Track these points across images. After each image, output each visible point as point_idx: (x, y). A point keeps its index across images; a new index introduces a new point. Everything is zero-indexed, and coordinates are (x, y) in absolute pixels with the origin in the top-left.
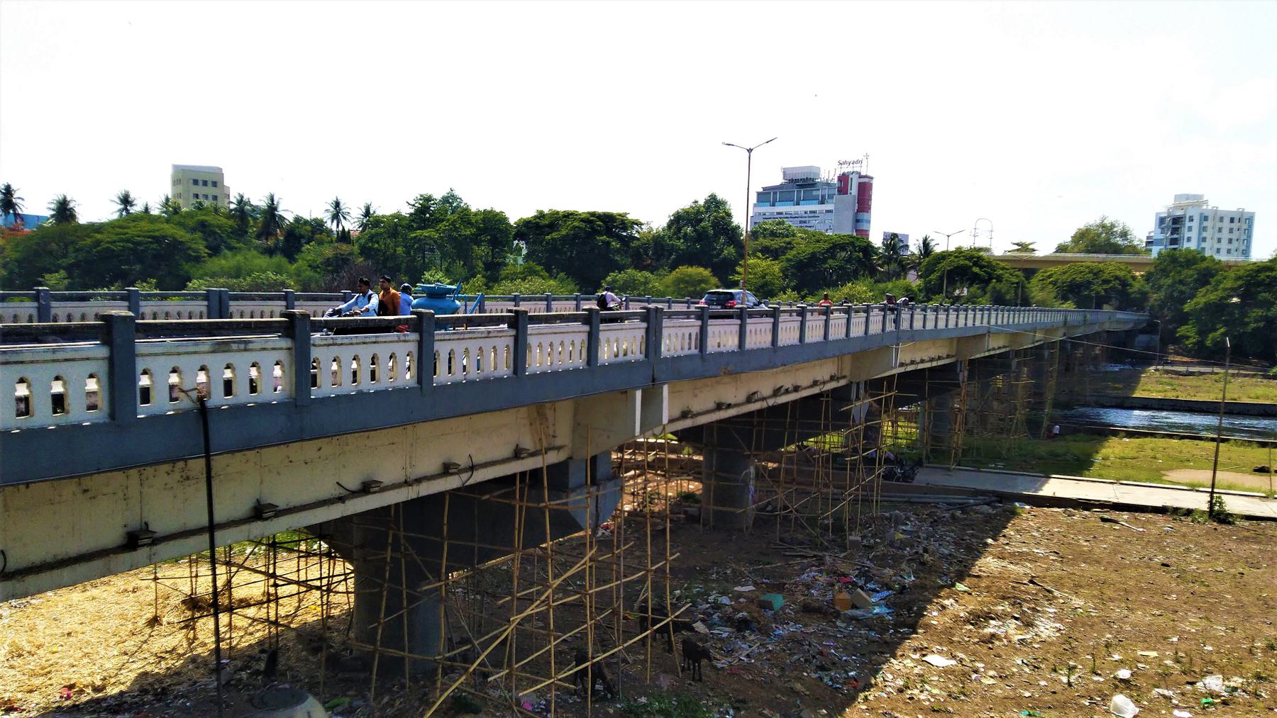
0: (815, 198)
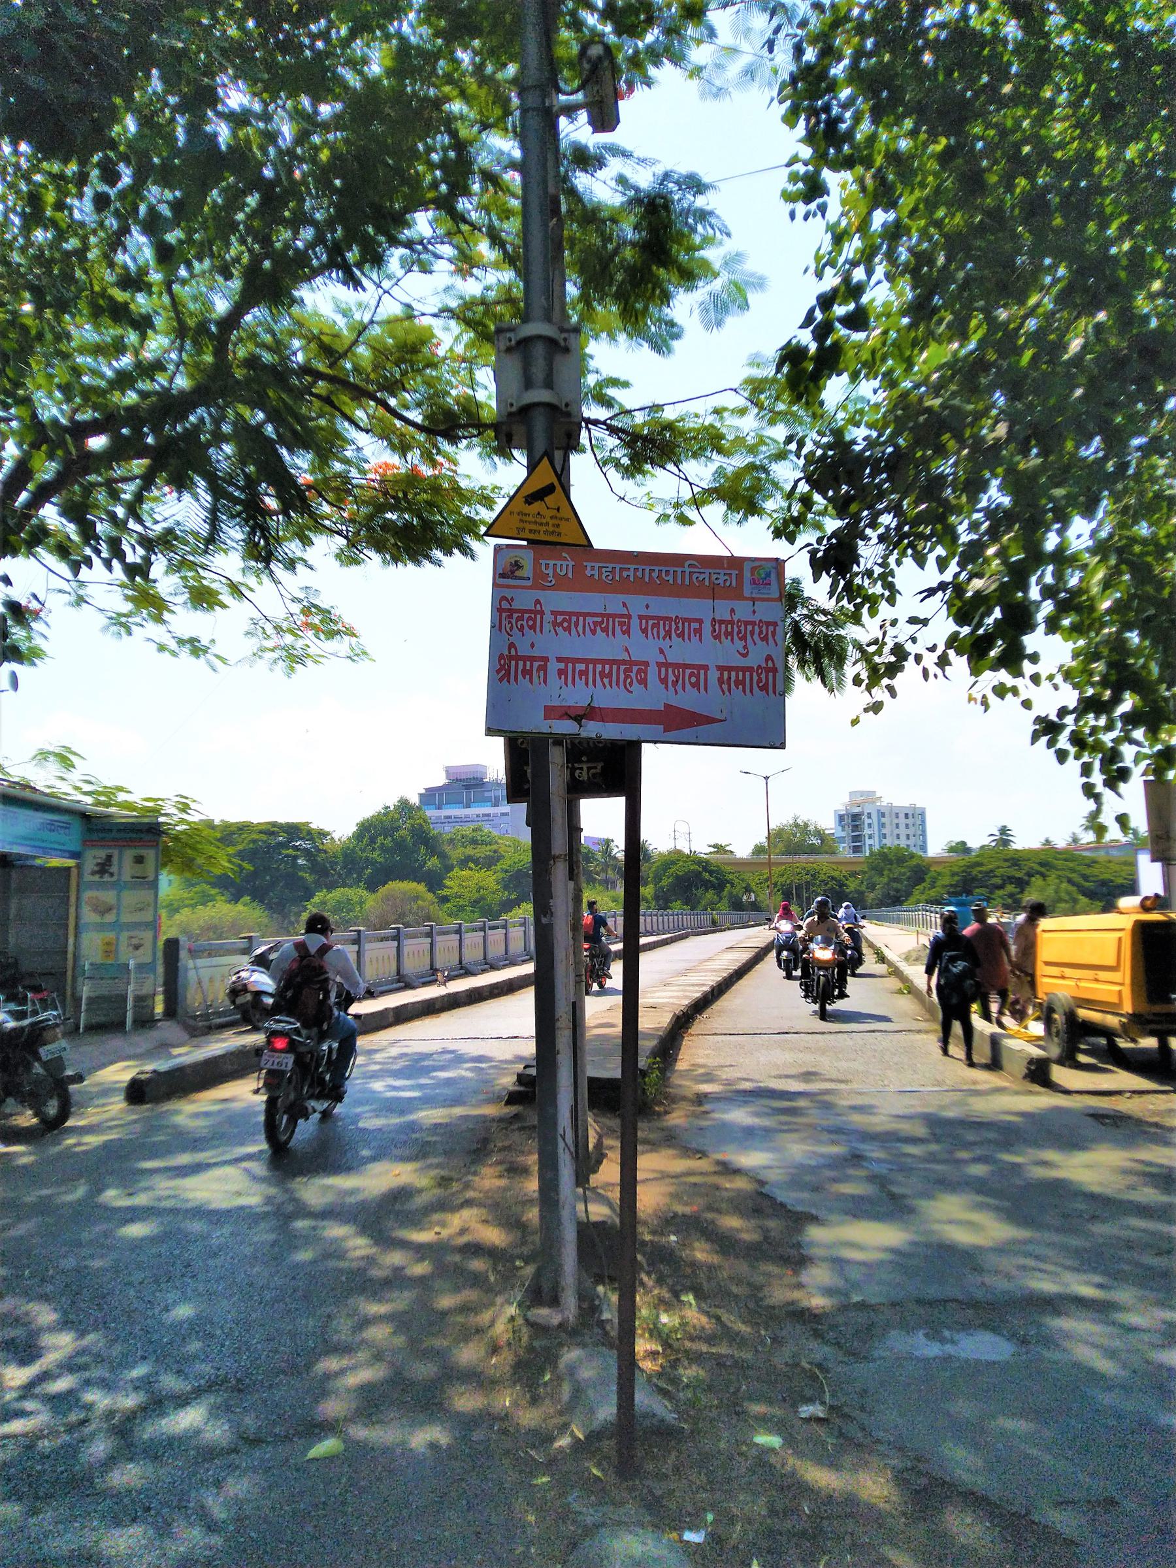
0: (488, 800)
